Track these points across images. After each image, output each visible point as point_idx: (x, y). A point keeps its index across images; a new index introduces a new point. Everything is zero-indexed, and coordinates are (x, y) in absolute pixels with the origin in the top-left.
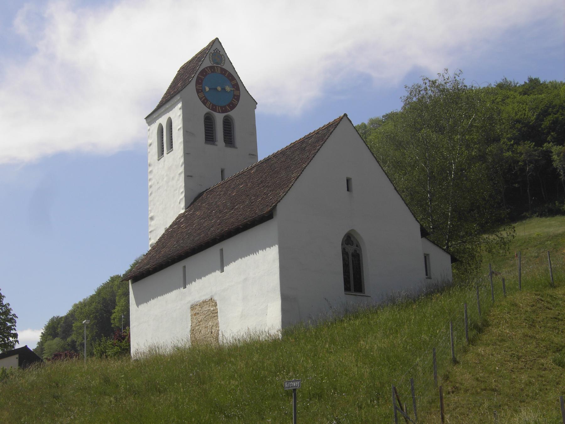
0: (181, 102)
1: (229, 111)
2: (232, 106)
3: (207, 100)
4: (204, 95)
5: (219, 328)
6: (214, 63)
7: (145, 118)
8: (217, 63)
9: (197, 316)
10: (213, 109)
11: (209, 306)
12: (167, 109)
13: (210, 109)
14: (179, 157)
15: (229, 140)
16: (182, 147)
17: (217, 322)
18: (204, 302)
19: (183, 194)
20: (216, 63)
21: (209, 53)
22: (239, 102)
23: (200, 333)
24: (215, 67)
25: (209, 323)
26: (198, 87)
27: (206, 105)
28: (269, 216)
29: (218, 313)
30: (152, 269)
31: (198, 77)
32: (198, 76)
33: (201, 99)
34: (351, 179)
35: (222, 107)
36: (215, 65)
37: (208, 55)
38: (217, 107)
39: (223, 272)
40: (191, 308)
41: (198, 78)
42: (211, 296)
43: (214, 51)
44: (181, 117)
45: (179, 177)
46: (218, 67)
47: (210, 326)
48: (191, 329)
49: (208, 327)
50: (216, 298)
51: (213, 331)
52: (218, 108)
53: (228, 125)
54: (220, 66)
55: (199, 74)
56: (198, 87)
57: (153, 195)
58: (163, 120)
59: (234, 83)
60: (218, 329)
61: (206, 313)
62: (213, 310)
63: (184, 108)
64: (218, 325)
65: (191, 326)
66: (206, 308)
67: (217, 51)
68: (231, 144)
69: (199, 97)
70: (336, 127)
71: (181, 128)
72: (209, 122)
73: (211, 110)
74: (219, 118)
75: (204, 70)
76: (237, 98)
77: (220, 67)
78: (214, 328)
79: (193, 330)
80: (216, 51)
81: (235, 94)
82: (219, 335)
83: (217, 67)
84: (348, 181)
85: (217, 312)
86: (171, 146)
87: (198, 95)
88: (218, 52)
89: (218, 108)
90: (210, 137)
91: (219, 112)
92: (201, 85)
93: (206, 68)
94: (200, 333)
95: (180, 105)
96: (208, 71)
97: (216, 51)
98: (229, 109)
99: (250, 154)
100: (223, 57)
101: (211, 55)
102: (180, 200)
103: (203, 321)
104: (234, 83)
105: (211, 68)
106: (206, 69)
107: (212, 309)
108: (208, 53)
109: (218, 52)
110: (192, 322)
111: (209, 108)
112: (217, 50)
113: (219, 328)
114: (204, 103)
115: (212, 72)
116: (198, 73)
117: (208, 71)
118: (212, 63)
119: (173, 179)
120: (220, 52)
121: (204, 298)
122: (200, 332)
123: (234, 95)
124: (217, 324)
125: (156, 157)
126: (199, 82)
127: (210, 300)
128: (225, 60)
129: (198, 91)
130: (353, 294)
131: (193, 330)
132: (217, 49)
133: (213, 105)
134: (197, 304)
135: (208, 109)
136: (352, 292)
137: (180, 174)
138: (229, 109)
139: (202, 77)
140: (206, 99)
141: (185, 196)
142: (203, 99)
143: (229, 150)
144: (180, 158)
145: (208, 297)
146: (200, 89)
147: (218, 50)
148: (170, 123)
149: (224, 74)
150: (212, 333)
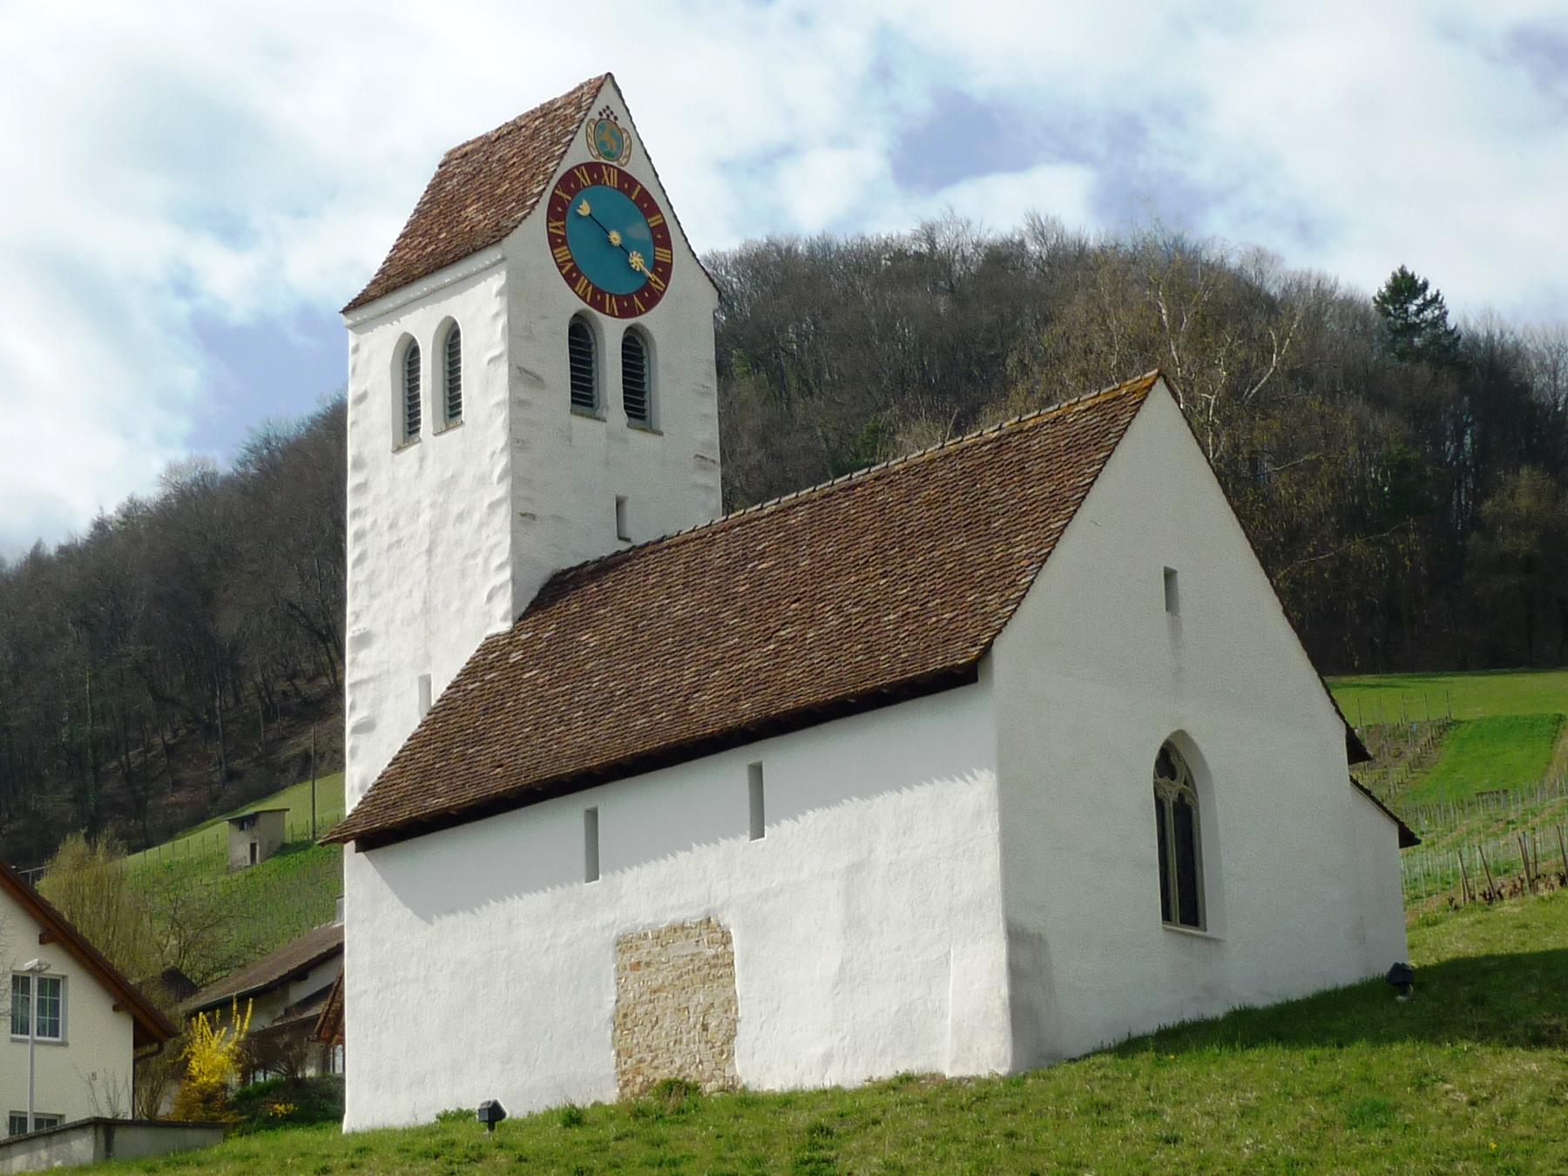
0: (504, 273)
1: (641, 313)
2: (650, 297)
3: (579, 274)
4: (569, 257)
5: (740, 1015)
6: (600, 154)
7: (341, 309)
8: (609, 155)
9: (644, 971)
10: (593, 303)
11: (697, 941)
12: (444, 287)
13: (586, 302)
14: (489, 450)
15: (637, 405)
16: (501, 418)
17: (732, 993)
18: (679, 929)
19: (507, 574)
20: (605, 154)
21: (586, 120)
22: (671, 282)
23: (653, 1027)
24: (604, 167)
25: (697, 995)
26: (553, 228)
27: (577, 289)
28: (964, 676)
29: (733, 964)
30: (457, 810)
31: (554, 194)
32: (553, 192)
33: (560, 268)
34: (1175, 572)
35: (619, 299)
36: (602, 160)
37: (584, 126)
38: (607, 296)
39: (763, 836)
40: (617, 945)
41: (554, 198)
42: (708, 911)
43: (601, 114)
44: (502, 321)
45: (489, 515)
46: (612, 166)
47: (699, 1008)
48: (618, 1011)
49: (691, 1011)
50: (730, 920)
51: (713, 1024)
52: (610, 300)
53: (635, 350)
54: (615, 164)
55: (556, 187)
56: (553, 228)
57: (368, 565)
58: (422, 324)
59: (654, 221)
60: (731, 1017)
61: (685, 965)
62: (716, 957)
63: (510, 292)
64: (732, 1003)
65: (617, 1001)
66: (683, 947)
67: (608, 116)
68: (643, 418)
69: (555, 259)
70: (1137, 410)
71: (500, 356)
72: (581, 338)
73: (589, 304)
74: (611, 331)
75: (570, 176)
76: (664, 270)
77: (614, 167)
78: (718, 1011)
79: (625, 1016)
80: (604, 116)
81: (658, 258)
82: (735, 1036)
83: (606, 165)
84: (1169, 575)
85: (733, 963)
86: (452, 408)
87: (553, 255)
88: (612, 118)
89: (610, 300)
90: (583, 395)
91: (612, 315)
92: (562, 223)
93: (577, 167)
94: (653, 1027)
95: (497, 281)
96: (582, 179)
97: (604, 116)
98: (641, 307)
99: (697, 456)
100: (625, 135)
101: (593, 126)
102: (493, 589)
103: (669, 988)
104: (654, 221)
105: (592, 168)
106: (576, 171)
107: (712, 952)
108: (582, 121)
109: (612, 118)
110: (622, 989)
111: (584, 298)
112: (608, 112)
113: (736, 1013)
114: (571, 279)
115: (595, 182)
116: (553, 182)
117: (582, 179)
118: (595, 153)
119: (461, 518)
120: (616, 118)
121: (672, 917)
122: (657, 1022)
123: (565, 242)
124: (731, 1001)
125: (385, 440)
126: (557, 211)
127: (701, 922)
128: (630, 146)
129: (555, 241)
130: (1175, 928)
131: (625, 1016)
132: (608, 107)
133: (596, 291)
134: (646, 935)
135: (581, 301)
136: (1177, 925)
137: (493, 506)
138: (641, 307)
139: (565, 196)
140: (575, 268)
141: (514, 579)
142: (567, 268)
143: (640, 439)
144: (493, 453)
145: (692, 915)
146: (559, 236)
147: (612, 113)
148: (451, 340)
149: (629, 193)
150: (705, 1028)
